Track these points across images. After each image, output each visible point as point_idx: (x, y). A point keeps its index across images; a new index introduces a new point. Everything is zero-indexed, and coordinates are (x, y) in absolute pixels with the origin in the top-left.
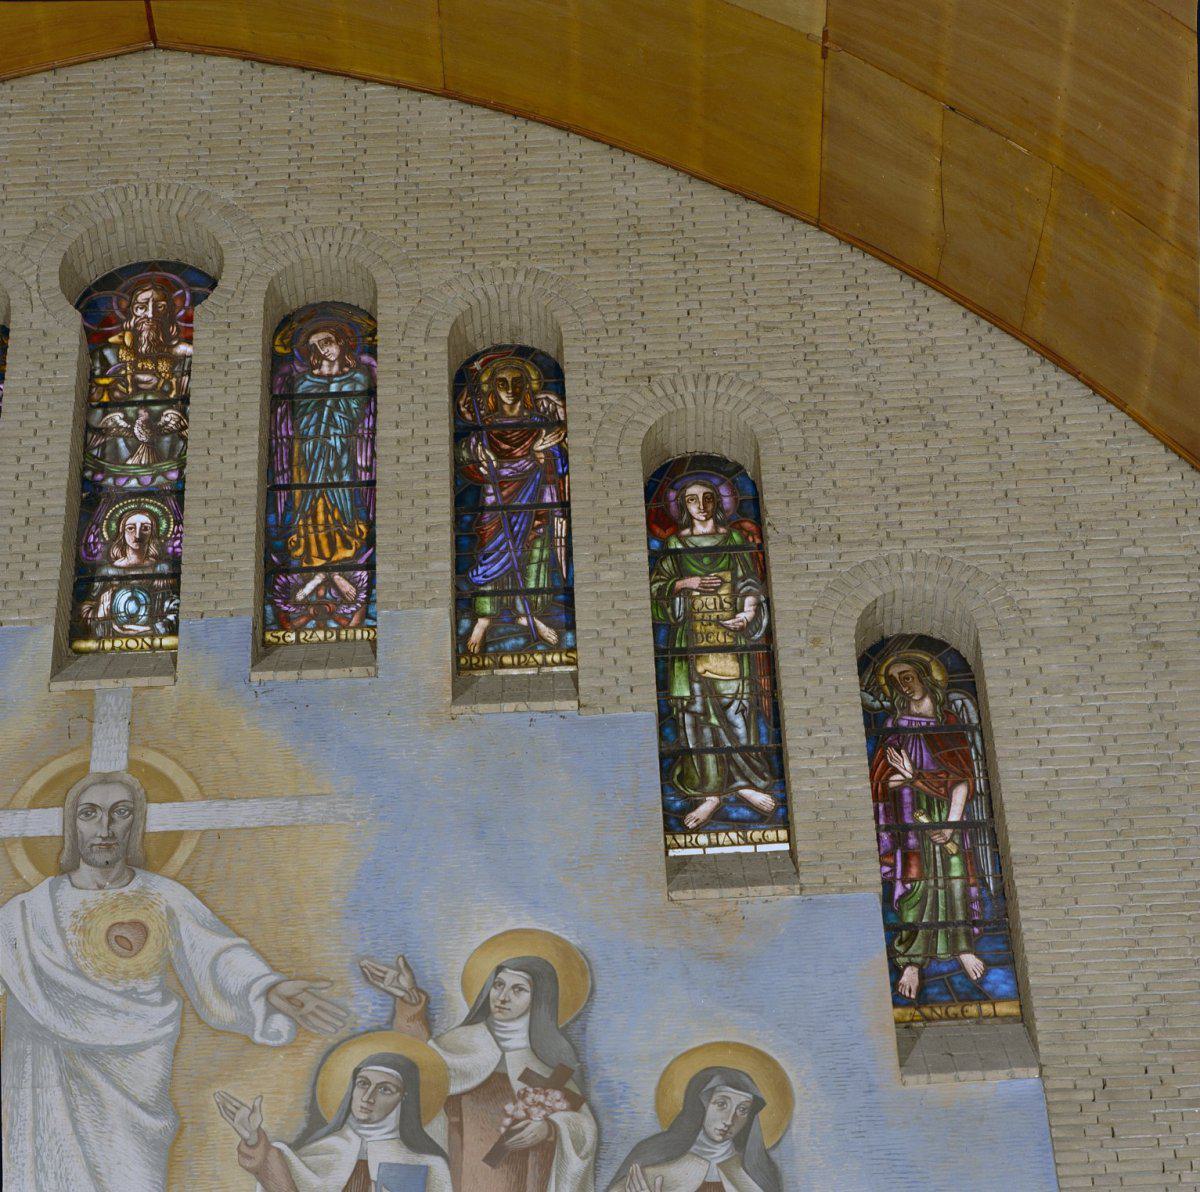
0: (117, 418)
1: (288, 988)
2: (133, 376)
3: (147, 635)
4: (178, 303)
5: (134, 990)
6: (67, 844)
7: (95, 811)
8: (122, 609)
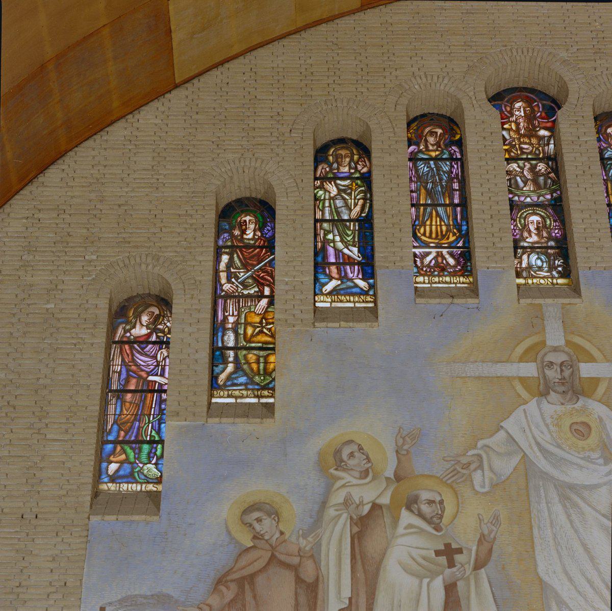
0: (514, 166)
2: (519, 145)
3: (550, 278)
4: (536, 109)
5: (589, 457)
6: (542, 381)
7: (552, 365)
8: (534, 264)
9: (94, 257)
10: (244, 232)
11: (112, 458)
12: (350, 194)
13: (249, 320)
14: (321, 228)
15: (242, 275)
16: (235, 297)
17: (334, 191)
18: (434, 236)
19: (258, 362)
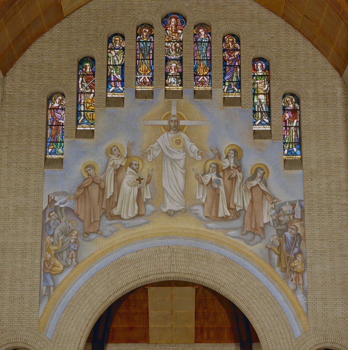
1: (201, 152)
4: (178, 22)
9: (42, 83)
10: (86, 69)
11: (50, 147)
12: (119, 55)
13: (88, 101)
14: (110, 68)
15: (86, 85)
16: (84, 93)
17: (114, 54)
18: (143, 71)
19: (90, 116)
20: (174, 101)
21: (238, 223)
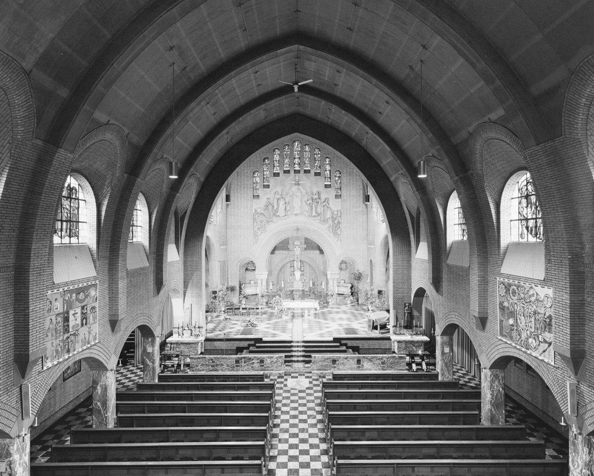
20: (297, 174)
21: (319, 218)
